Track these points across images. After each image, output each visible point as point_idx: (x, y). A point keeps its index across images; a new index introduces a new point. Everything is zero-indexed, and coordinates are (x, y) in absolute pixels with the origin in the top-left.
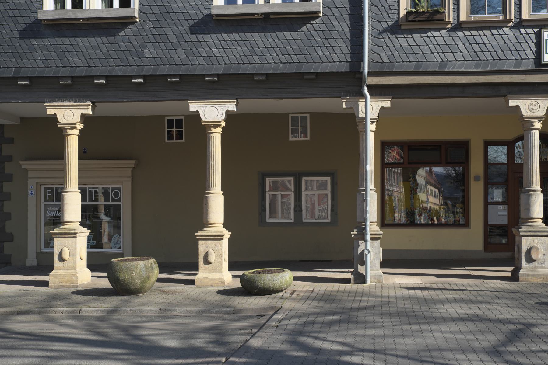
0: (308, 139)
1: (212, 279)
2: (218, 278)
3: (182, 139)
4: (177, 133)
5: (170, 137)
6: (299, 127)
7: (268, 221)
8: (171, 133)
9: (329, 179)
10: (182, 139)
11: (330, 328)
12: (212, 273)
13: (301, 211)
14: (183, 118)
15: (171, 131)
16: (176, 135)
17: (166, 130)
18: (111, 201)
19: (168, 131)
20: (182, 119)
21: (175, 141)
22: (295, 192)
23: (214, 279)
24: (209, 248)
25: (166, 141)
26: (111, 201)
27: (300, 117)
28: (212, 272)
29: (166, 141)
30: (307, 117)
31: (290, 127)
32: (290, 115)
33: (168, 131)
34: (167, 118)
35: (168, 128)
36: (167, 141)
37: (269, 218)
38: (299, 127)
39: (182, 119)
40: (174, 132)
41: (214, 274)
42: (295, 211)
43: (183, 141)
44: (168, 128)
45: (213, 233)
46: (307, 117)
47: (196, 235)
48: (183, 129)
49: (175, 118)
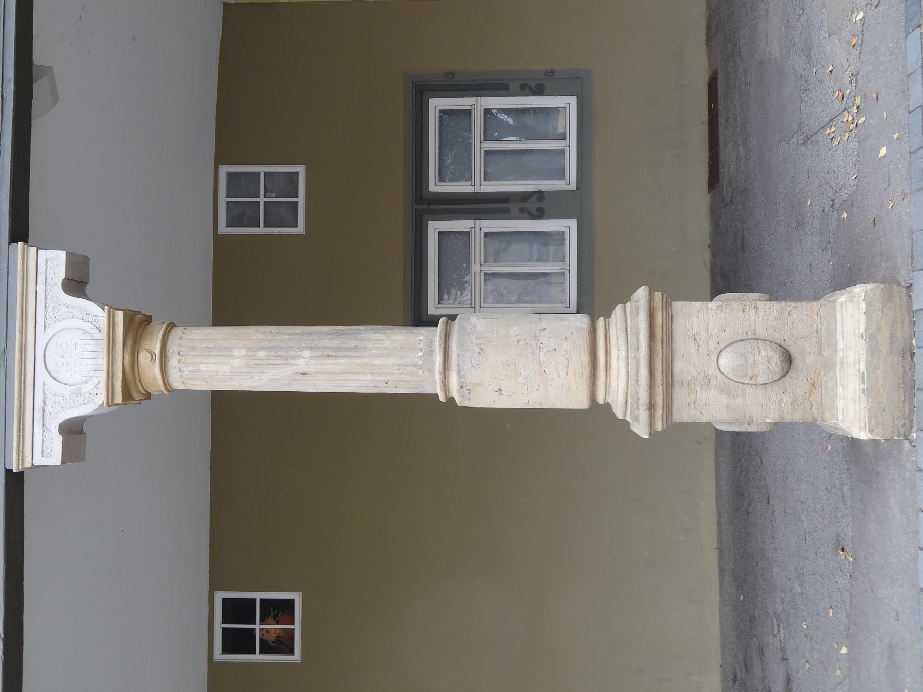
0: (301, 170)
1: (873, 351)
2: (863, 318)
3: (291, 602)
4: (271, 619)
5: (284, 644)
6: (258, 626)
7: (573, 186)
8: (273, 642)
9: (436, 105)
10: (291, 602)
11: (854, 296)
12: (840, 354)
13: (540, 195)
14: (219, 596)
15: (261, 639)
16: (278, 623)
17: (258, 657)
18: (255, 600)
19: (262, 652)
20: (225, 601)
21: (297, 627)
22: (477, 215)
23: (871, 339)
24: (712, 371)
25: (296, 657)
26: (255, 600)
27: (227, 197)
28: (835, 351)
29: (296, 657)
30: (229, 175)
31: (262, 230)
32: (223, 229)
33: (262, 652)
34: (218, 655)
35: (254, 652)
36: (296, 657)
37: (564, 182)
38: (262, 200)
39: (225, 601)
40: (268, 631)
41: (841, 345)
42: (539, 215)
43: (296, 596)
44: (254, 652)
45: (638, 349)
46: (229, 175)
47: (650, 434)
48: (259, 596)
49: (218, 626)
